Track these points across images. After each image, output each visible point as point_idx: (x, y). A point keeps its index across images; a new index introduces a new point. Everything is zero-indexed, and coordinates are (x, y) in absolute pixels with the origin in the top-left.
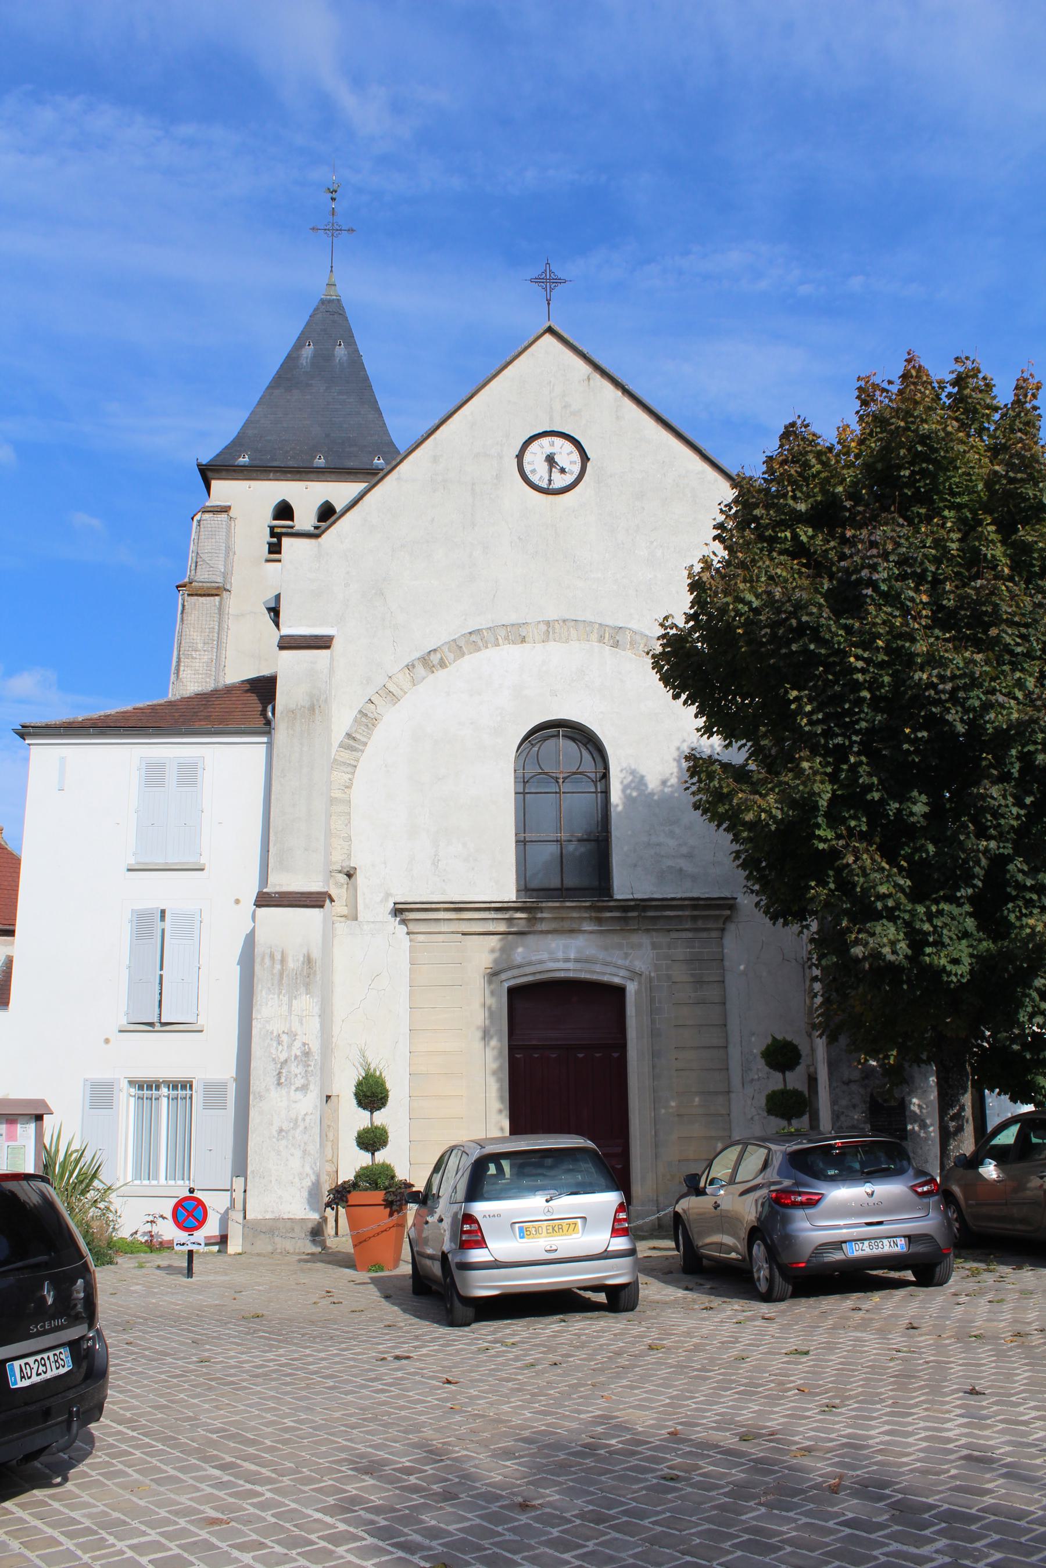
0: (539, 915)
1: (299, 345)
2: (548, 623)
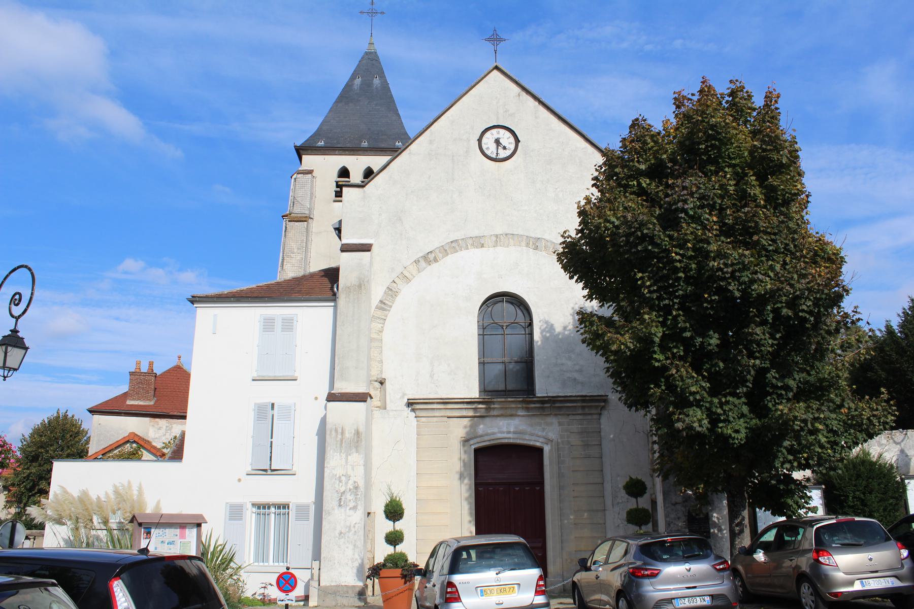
0: (492, 406)
2: (497, 236)
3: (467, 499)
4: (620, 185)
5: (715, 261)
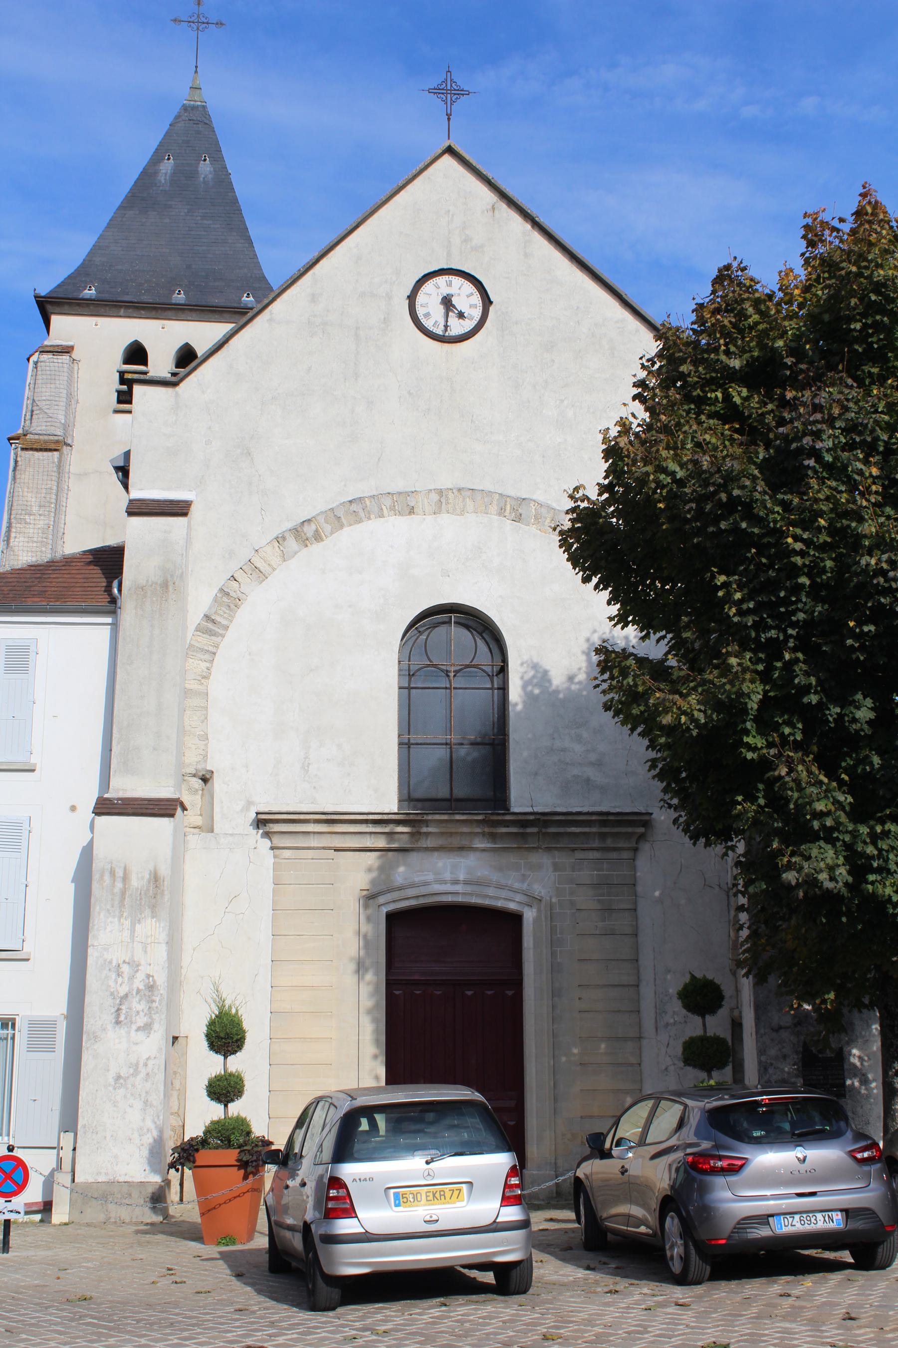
0: (424, 830)
1: (157, 158)
2: (440, 492)
3: (369, 1012)
4: (688, 398)
5: (871, 556)
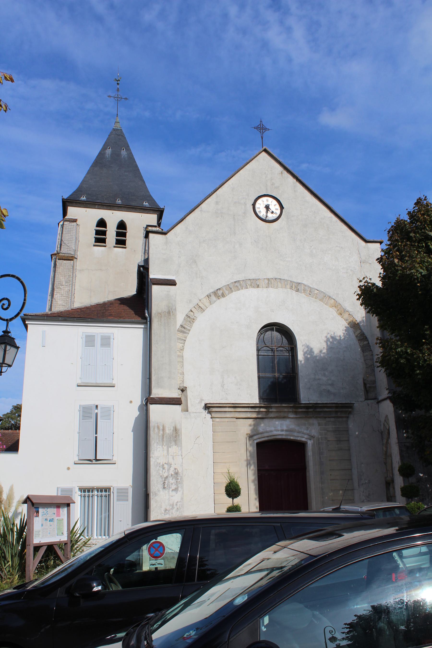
0: (271, 410)
1: (104, 148)
2: (268, 279)
3: (253, 481)
